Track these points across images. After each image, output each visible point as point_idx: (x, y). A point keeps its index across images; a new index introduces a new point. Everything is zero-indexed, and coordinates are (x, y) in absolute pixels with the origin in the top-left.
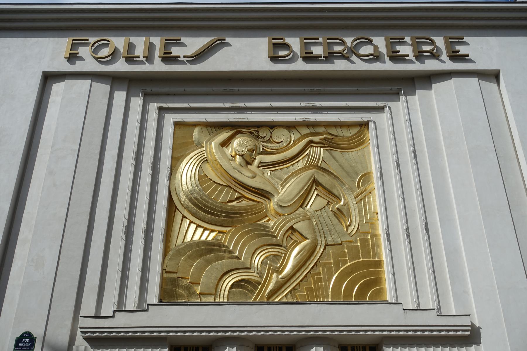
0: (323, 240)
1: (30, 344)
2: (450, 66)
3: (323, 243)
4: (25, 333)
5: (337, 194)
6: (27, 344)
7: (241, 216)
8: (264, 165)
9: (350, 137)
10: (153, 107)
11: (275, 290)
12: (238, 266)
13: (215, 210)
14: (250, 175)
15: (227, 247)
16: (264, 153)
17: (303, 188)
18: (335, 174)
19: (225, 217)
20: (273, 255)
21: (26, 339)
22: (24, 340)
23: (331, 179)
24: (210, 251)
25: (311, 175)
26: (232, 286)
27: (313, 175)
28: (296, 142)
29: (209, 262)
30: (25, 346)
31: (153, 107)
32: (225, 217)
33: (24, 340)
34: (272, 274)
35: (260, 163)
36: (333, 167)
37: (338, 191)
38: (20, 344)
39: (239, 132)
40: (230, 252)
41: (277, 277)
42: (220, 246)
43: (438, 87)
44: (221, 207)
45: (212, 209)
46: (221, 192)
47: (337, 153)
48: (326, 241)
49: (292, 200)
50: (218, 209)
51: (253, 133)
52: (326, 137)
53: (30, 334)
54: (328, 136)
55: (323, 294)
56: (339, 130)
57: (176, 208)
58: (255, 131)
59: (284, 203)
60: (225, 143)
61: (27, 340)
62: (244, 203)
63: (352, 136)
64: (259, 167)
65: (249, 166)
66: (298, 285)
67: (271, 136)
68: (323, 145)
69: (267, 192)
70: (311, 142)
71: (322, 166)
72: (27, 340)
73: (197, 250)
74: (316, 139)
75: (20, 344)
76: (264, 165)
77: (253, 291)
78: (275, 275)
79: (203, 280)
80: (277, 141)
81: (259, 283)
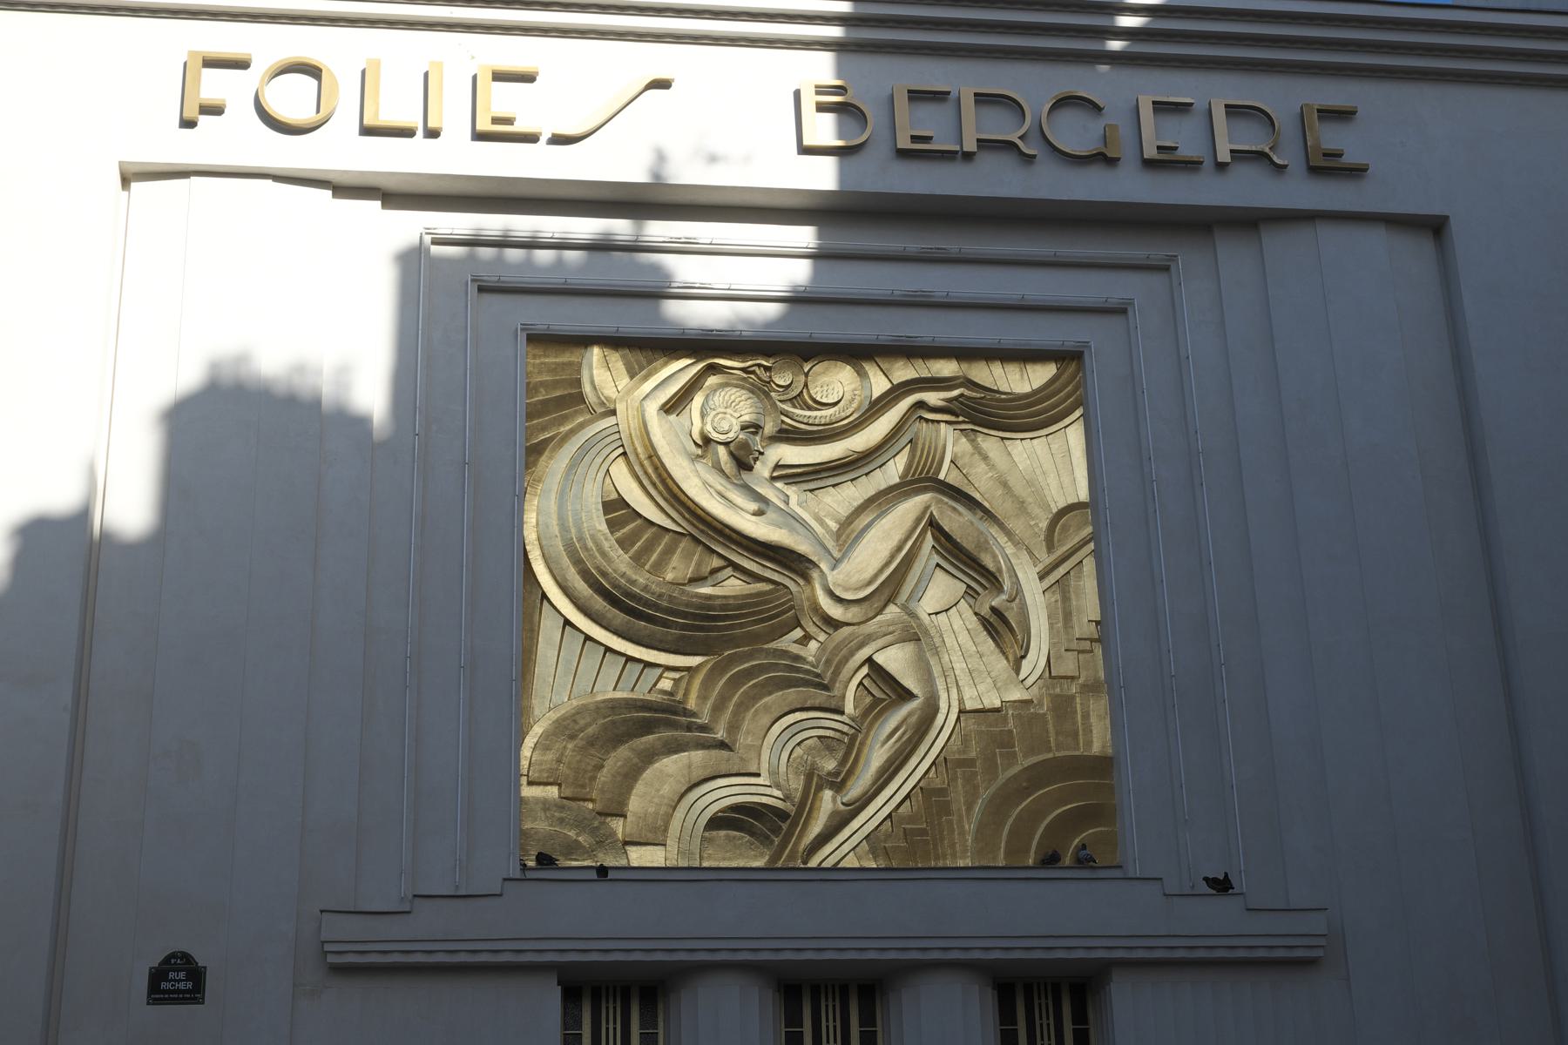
0: (954, 695)
1: (190, 985)
2: (1301, 193)
3: (955, 704)
4: (173, 955)
5: (991, 566)
6: (182, 986)
7: (731, 627)
8: (789, 475)
9: (1027, 396)
10: (679, 697)
11: (888, 502)
12: (724, 769)
13: (656, 607)
14: (753, 506)
15: (694, 714)
16: (788, 435)
17: (899, 549)
18: (986, 504)
19: (684, 627)
20: (819, 737)
21: (178, 971)
22: (171, 975)
23: (975, 520)
24: (647, 727)
25: (921, 508)
26: (715, 823)
27: (927, 508)
28: (877, 407)
29: (649, 757)
30: (178, 991)
31: (679, 697)
32: (684, 627)
33: (171, 975)
34: (820, 788)
35: (777, 466)
36: (981, 484)
37: (994, 556)
38: (164, 985)
39: (713, 369)
40: (703, 728)
41: (834, 800)
42: (675, 713)
43: (1275, 242)
44: (671, 599)
45: (647, 603)
46: (669, 552)
47: (990, 443)
48: (961, 701)
49: (870, 583)
50: (665, 604)
51: (753, 372)
52: (962, 395)
53: (186, 958)
54: (967, 393)
55: (953, 845)
56: (997, 369)
57: (544, 596)
58: (759, 365)
59: (846, 589)
60: (674, 406)
61: (182, 975)
62: (733, 586)
63: (1035, 392)
64: (773, 479)
65: (745, 476)
66: (888, 823)
67: (806, 385)
68: (952, 418)
69: (802, 558)
70: (921, 405)
71: (950, 480)
72: (182, 975)
73: (613, 722)
74: (933, 398)
75: (164, 985)
76: (789, 475)
77: (768, 838)
78: (828, 794)
79: (635, 804)
80: (824, 400)
81: (782, 815)
